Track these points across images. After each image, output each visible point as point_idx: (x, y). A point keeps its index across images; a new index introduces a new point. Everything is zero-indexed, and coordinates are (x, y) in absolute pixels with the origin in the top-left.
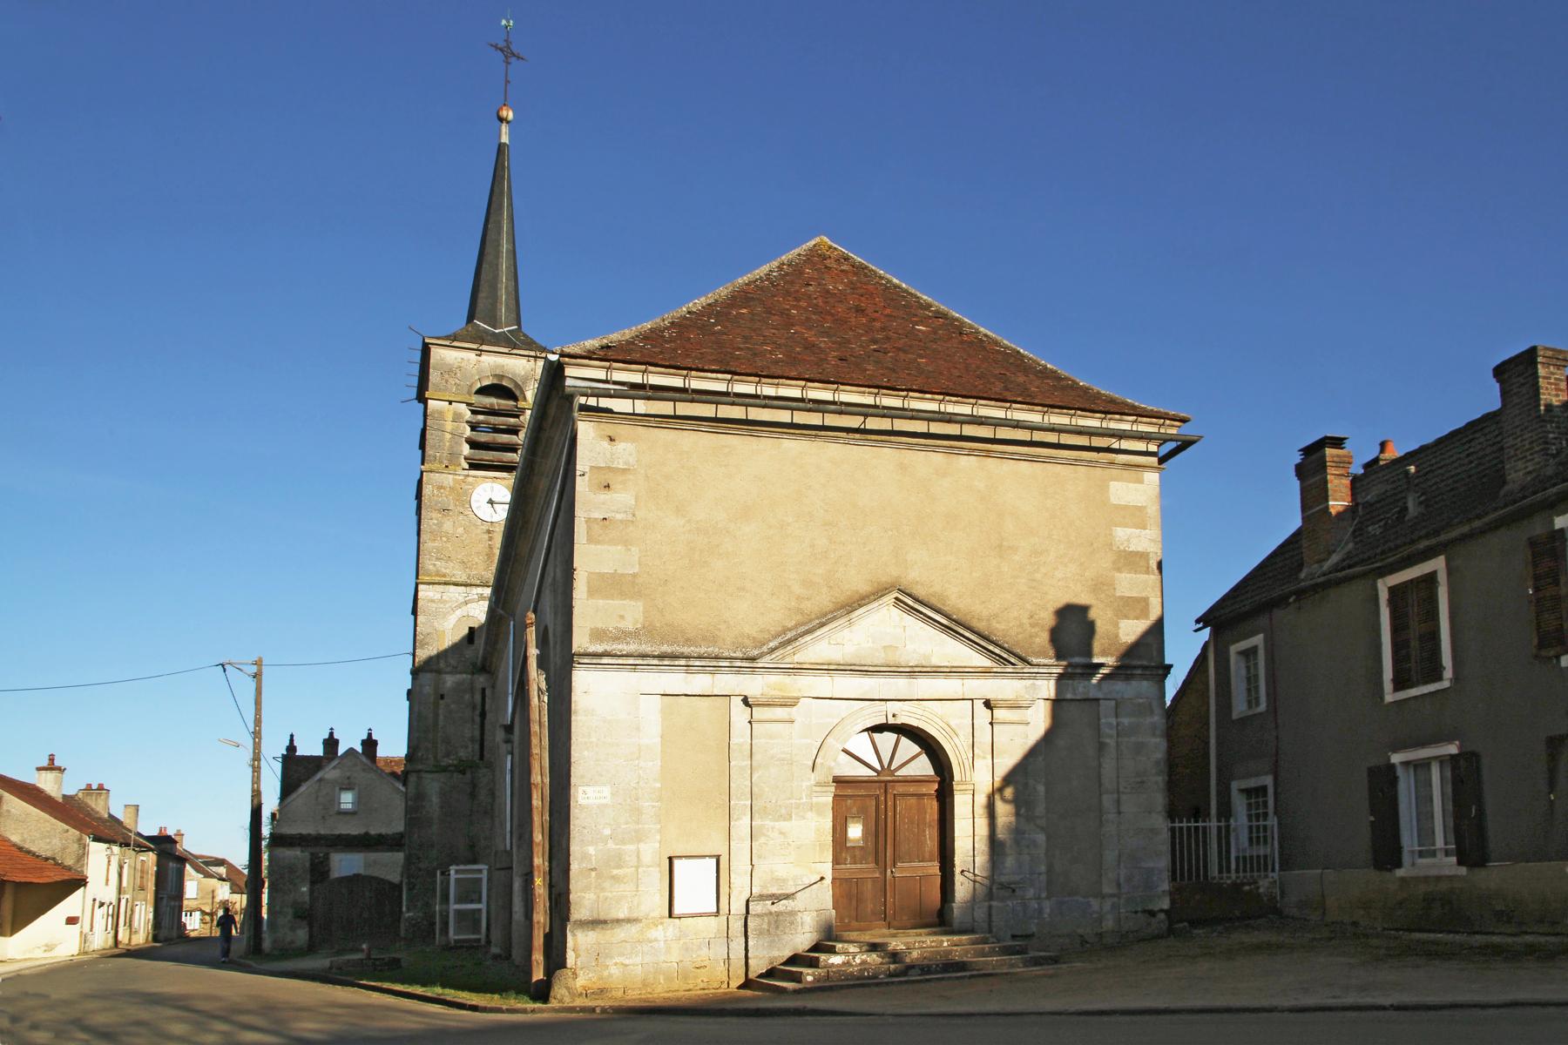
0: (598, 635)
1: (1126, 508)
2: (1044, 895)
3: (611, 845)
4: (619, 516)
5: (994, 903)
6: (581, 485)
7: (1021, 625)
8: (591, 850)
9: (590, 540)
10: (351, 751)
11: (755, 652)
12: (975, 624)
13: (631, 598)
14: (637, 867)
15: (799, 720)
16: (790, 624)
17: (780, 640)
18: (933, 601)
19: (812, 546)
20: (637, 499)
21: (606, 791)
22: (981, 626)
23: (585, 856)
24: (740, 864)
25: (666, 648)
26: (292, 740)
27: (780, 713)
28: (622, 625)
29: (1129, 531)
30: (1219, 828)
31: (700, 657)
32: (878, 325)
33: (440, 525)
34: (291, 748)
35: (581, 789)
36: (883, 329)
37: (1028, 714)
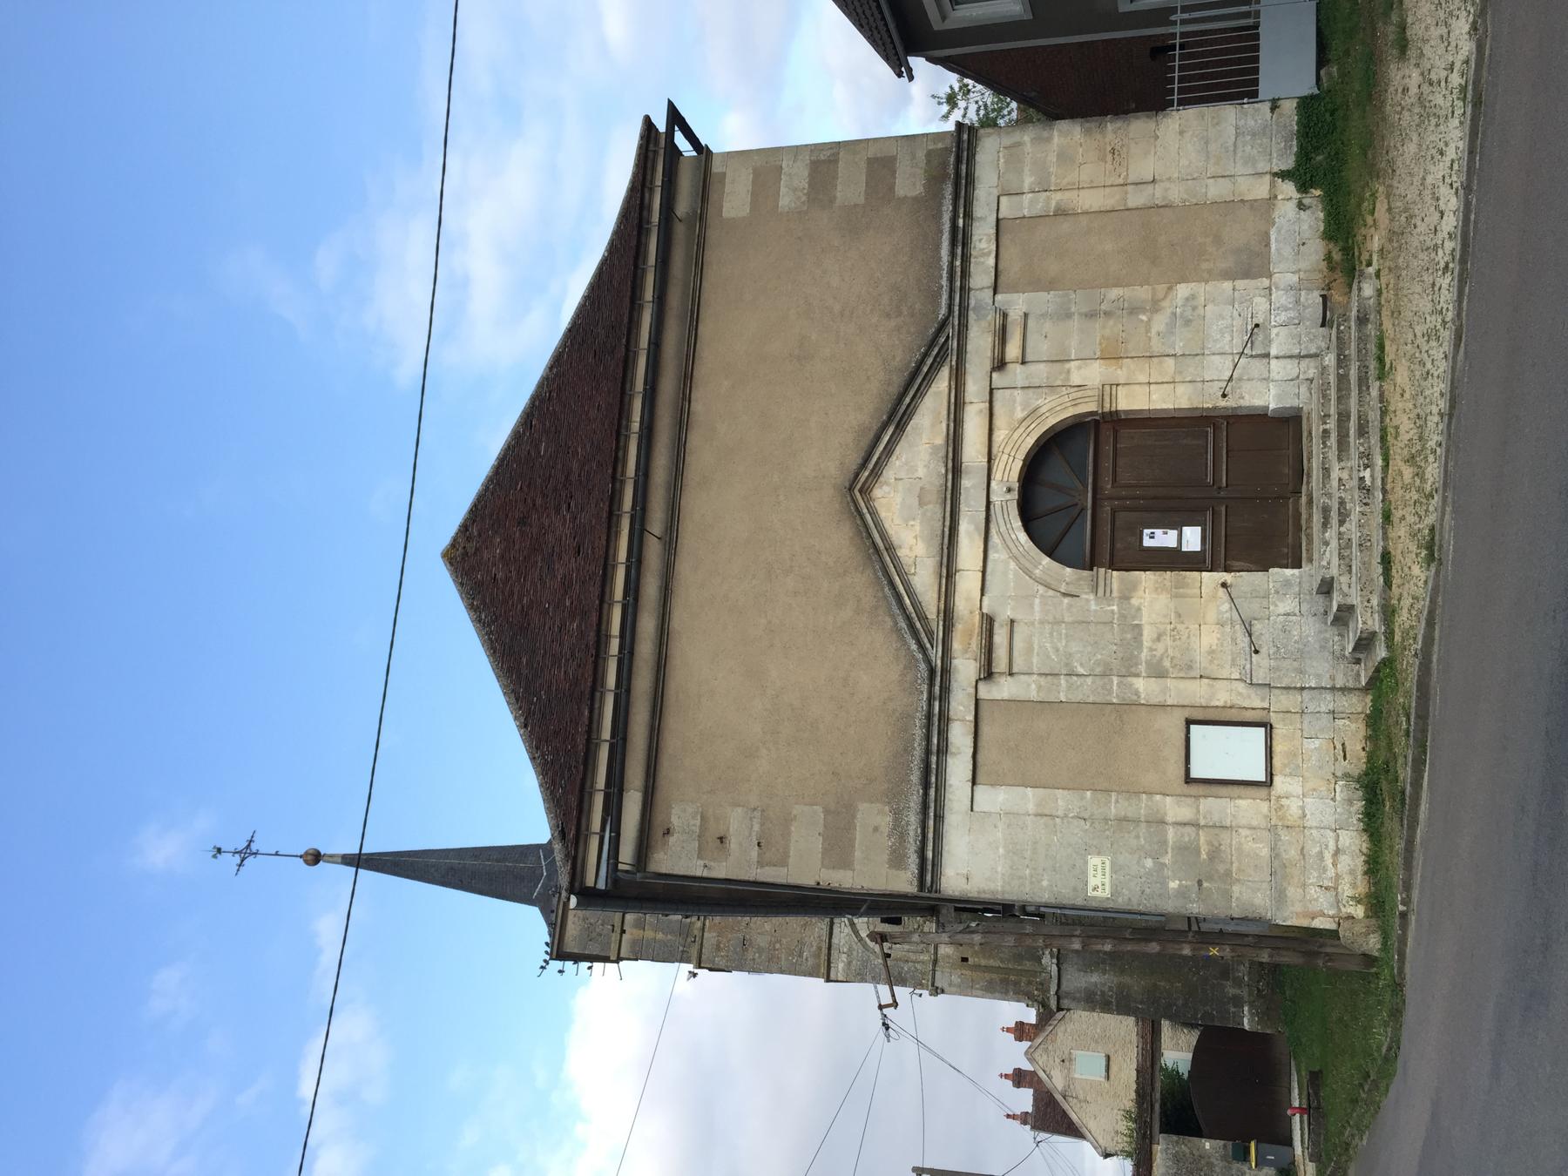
0: (897, 861)
1: (754, 194)
2: (1266, 282)
3: (1167, 859)
4: (756, 827)
5: (1273, 352)
6: (720, 871)
7: (898, 329)
8: (1174, 885)
9: (783, 862)
10: (1029, 1055)
11: (923, 666)
12: (894, 390)
13: (854, 817)
14: (1196, 825)
15: (1009, 613)
16: (889, 623)
17: (908, 637)
18: (865, 442)
19: (796, 593)
20: (736, 805)
21: (1094, 861)
22: (898, 381)
23: (1182, 893)
24: (1196, 693)
25: (915, 777)
26: (1013, 1117)
27: (1000, 638)
28: (885, 830)
29: (783, 190)
30: (1173, 36)
31: (928, 738)
32: (539, 501)
33: (760, 950)
34: (1024, 1118)
35: (1090, 893)
36: (544, 496)
37: (1015, 315)
